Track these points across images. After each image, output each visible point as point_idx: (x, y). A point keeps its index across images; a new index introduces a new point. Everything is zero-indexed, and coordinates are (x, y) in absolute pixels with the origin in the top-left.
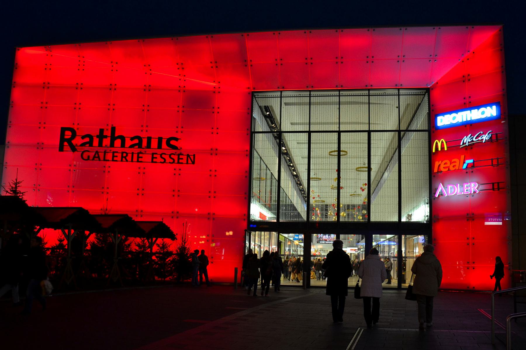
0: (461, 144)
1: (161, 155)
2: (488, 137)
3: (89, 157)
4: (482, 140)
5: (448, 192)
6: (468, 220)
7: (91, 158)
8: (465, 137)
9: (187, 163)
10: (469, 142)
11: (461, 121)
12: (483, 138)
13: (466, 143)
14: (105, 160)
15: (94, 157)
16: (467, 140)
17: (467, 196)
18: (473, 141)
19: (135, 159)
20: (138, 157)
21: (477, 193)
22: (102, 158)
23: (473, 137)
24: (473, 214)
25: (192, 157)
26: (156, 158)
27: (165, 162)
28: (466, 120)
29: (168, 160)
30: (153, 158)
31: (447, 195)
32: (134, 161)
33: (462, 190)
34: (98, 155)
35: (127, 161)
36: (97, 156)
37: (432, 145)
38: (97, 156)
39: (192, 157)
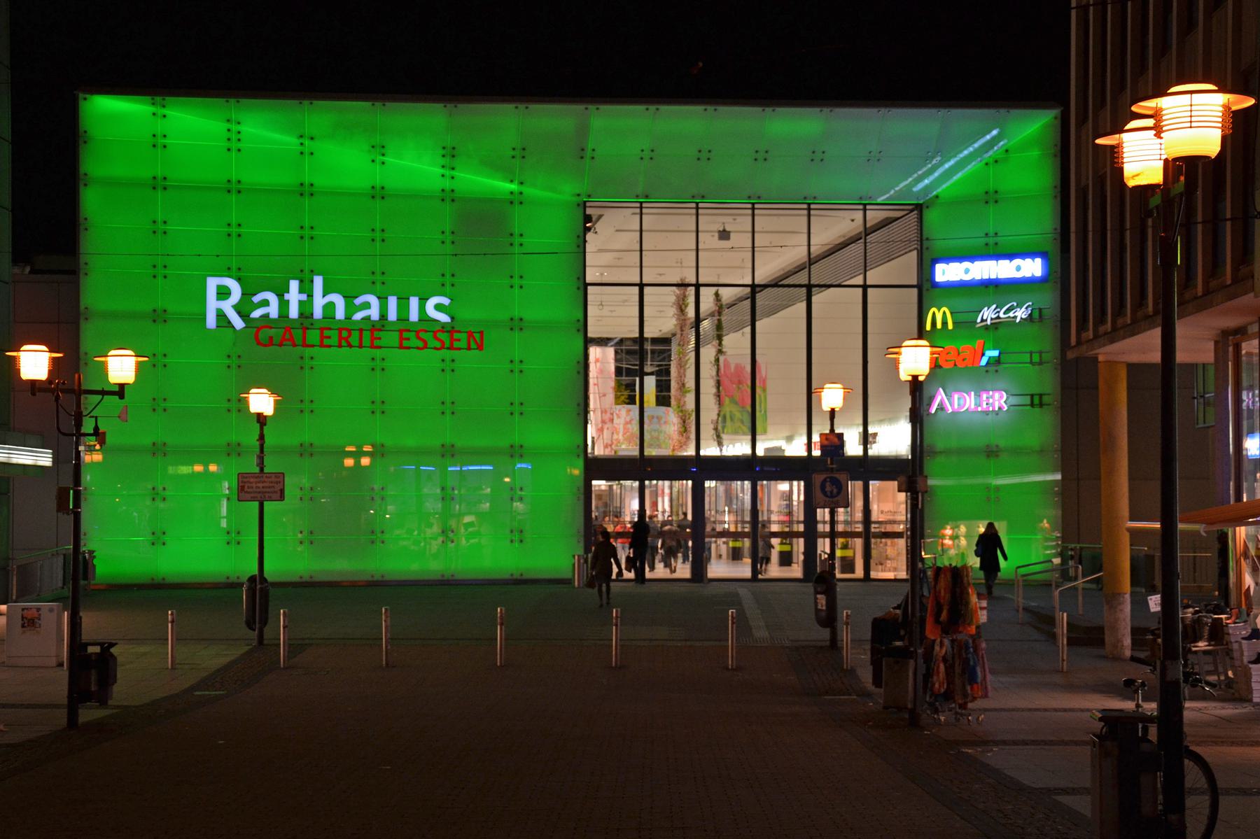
0: (979, 320)
1: (418, 333)
2: (1025, 313)
3: (271, 338)
4: (1015, 317)
5: (952, 405)
6: (988, 456)
7: (276, 341)
8: (986, 308)
9: (469, 348)
10: (992, 319)
11: (980, 278)
12: (1016, 314)
13: (986, 320)
14: (305, 345)
15: (283, 339)
16: (988, 314)
17: (986, 413)
18: (998, 317)
19: (367, 341)
20: (373, 339)
21: (1005, 410)
22: (299, 340)
23: (999, 310)
24: (997, 446)
25: (477, 336)
26: (408, 339)
27: (425, 347)
28: (988, 278)
29: (433, 343)
30: (402, 339)
31: (950, 411)
32: (364, 345)
33: (978, 403)
34: (291, 334)
35: (350, 345)
36: (287, 336)
37: (924, 319)
38: (287, 336)
39: (477, 336)
